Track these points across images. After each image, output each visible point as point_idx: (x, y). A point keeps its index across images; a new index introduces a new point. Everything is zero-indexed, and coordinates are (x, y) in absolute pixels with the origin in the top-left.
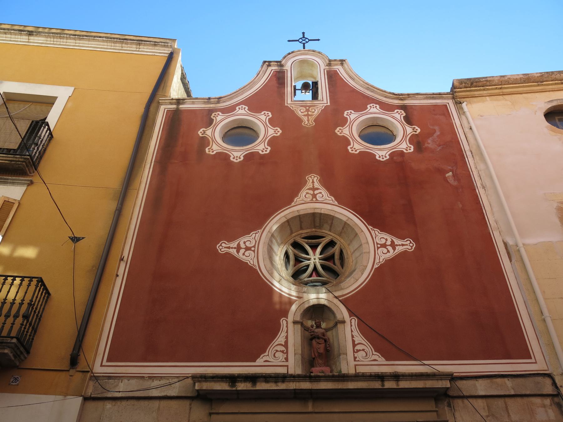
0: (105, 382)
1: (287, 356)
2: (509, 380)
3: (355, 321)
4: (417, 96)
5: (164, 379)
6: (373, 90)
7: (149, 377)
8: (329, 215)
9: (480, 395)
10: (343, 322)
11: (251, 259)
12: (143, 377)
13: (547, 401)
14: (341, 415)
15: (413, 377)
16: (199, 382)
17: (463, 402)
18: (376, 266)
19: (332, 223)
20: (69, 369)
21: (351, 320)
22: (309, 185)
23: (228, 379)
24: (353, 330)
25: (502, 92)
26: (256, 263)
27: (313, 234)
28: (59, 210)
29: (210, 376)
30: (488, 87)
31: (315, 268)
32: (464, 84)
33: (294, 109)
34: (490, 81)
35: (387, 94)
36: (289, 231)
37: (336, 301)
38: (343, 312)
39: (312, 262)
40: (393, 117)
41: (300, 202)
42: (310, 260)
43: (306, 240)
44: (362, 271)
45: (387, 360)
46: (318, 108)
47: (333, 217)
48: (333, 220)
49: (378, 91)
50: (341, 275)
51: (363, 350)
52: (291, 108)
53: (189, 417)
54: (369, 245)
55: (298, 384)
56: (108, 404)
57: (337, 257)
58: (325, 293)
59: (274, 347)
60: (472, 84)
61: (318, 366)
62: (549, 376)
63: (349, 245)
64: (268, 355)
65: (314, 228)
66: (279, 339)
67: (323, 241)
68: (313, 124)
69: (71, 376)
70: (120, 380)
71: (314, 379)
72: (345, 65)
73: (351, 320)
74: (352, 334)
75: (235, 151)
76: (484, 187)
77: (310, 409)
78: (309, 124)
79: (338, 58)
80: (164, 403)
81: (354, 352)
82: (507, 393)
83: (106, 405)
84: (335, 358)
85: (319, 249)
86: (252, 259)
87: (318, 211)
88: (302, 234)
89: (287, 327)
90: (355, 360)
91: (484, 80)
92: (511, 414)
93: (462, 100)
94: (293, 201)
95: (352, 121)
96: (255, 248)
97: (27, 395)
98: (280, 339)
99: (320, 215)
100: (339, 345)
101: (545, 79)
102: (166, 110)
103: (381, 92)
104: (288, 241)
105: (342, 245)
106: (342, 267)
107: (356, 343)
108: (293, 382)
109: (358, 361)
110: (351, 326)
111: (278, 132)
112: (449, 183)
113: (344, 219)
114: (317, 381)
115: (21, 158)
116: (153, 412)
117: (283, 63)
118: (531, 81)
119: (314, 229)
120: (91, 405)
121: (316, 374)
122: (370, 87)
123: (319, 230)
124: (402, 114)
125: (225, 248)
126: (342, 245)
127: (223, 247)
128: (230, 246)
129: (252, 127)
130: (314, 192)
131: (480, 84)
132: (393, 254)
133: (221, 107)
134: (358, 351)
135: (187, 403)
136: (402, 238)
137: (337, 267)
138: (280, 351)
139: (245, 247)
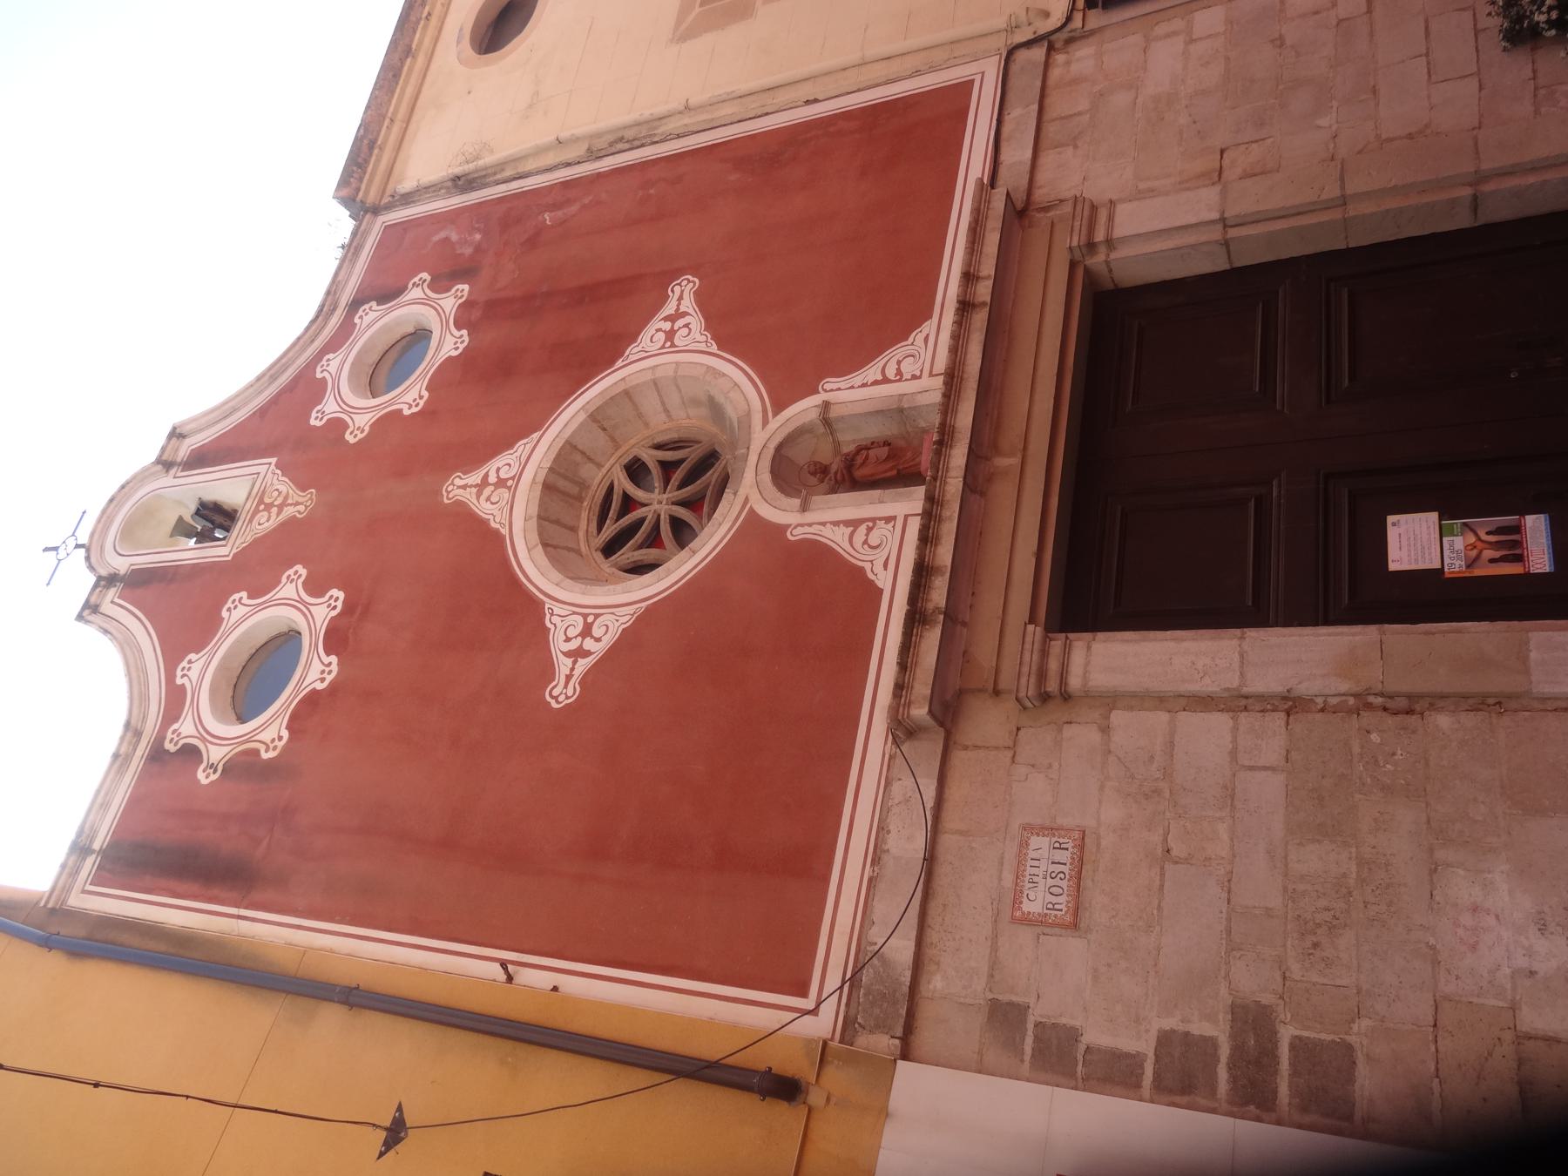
0: (865, 995)
1: (880, 519)
2: (1009, 114)
3: (830, 383)
5: (886, 820)
7: (873, 863)
8: (559, 451)
9: (1031, 157)
10: (826, 405)
11: (617, 621)
12: (870, 880)
15: (976, 248)
18: (714, 348)
19: (583, 453)
20: (807, 1109)
21: (825, 391)
22: (469, 496)
24: (850, 385)
26: (631, 609)
27: (597, 509)
28: (276, 1112)
31: (682, 503)
33: (249, 539)
35: (306, 337)
36: (572, 555)
38: (804, 409)
39: (667, 507)
40: (369, 326)
41: (504, 515)
42: (659, 516)
44: (717, 375)
45: (929, 317)
46: (272, 484)
47: (568, 442)
50: (713, 444)
51: (899, 363)
52: (244, 545)
53: (997, 748)
54: (657, 366)
55: (952, 473)
56: (931, 987)
59: (855, 550)
60: (359, 166)
61: (917, 460)
62: (1011, 52)
63: (646, 425)
64: (871, 561)
65: (582, 503)
66: (838, 539)
67: (619, 484)
68: (312, 493)
71: (946, 437)
72: (185, 430)
73: (825, 391)
74: (859, 387)
75: (303, 678)
78: (307, 501)
80: (951, 819)
81: (900, 380)
82: (1034, 115)
84: (907, 432)
85: (638, 494)
86: (618, 618)
87: (541, 478)
88: (587, 531)
89: (810, 525)
90: (920, 377)
92: (1076, 111)
93: (389, 191)
94: (497, 532)
95: (341, 408)
98: (837, 538)
99: (553, 473)
100: (877, 412)
102: (117, 600)
103: (297, 348)
104: (596, 562)
105: (642, 443)
106: (698, 442)
108: (945, 483)
109: (921, 371)
110: (839, 389)
113: (582, 416)
114: (953, 433)
116: (972, 848)
117: (104, 573)
119: (585, 504)
120: (925, 1037)
121: (936, 430)
122: (272, 372)
123: (591, 493)
124: (241, 598)
125: (566, 687)
126: (642, 443)
127: (562, 691)
128: (567, 676)
130: (491, 484)
132: (695, 316)
134: (899, 372)
135: (959, 758)
136: (664, 299)
137: (692, 455)
138: (867, 535)
139: (580, 639)
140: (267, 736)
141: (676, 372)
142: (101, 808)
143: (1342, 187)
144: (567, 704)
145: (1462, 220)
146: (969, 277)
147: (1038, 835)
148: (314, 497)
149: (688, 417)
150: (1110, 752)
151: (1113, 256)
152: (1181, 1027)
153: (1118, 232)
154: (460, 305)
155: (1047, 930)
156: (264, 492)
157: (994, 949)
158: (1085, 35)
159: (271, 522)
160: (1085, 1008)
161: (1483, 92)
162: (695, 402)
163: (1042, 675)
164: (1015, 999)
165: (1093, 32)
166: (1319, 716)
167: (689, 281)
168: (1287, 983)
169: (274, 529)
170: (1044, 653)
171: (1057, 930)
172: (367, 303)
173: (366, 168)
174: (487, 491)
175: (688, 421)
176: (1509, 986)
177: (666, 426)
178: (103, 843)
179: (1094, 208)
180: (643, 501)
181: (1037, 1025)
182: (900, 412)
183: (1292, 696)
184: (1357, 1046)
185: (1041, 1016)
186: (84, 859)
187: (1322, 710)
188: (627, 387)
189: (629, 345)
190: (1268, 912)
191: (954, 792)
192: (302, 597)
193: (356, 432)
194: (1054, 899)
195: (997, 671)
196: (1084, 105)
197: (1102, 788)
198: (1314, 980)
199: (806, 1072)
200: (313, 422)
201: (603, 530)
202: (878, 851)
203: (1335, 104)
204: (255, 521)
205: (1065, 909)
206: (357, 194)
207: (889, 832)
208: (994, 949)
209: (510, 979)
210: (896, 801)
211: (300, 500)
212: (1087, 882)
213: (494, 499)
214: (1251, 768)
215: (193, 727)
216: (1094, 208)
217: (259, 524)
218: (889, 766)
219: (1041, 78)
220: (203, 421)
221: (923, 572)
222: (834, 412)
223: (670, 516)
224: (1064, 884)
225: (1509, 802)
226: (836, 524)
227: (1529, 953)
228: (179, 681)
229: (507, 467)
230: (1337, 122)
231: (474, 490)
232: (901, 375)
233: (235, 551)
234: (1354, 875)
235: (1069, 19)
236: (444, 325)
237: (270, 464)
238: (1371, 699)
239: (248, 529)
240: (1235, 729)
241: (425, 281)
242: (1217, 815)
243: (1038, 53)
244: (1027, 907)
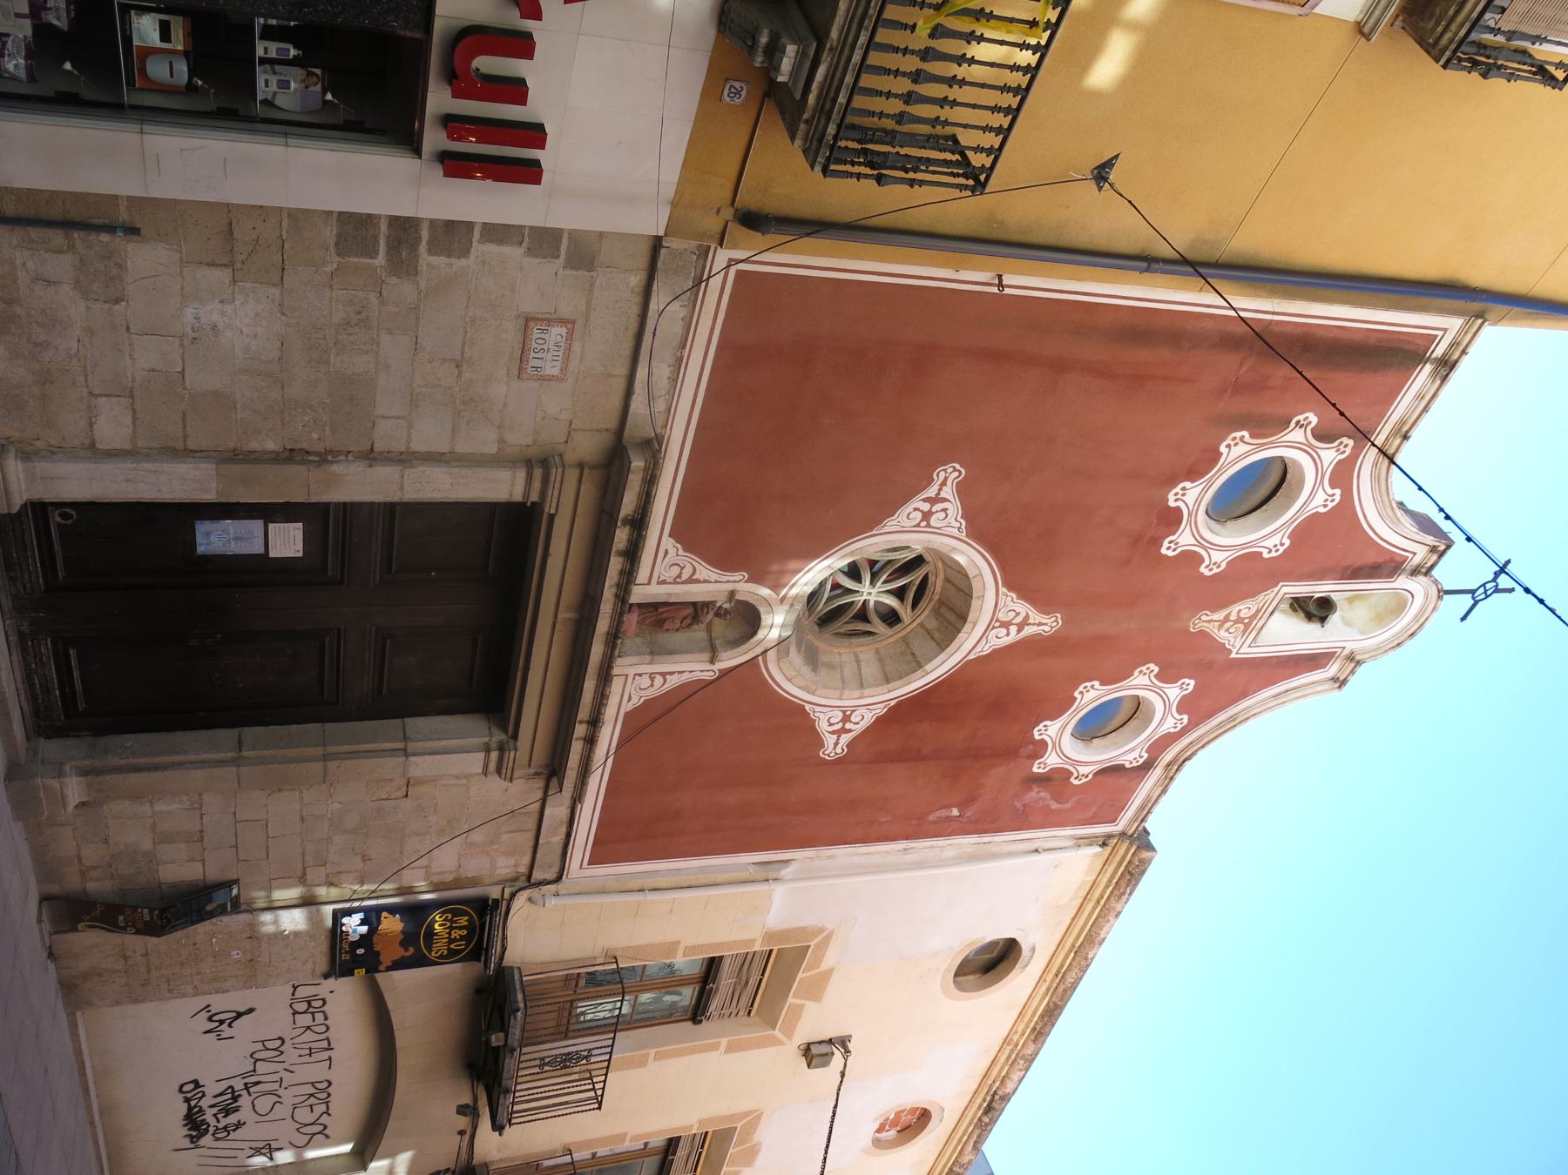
0: (690, 273)
1: (670, 583)
3: (708, 676)
4: (1161, 788)
6: (1221, 728)
7: (682, 358)
10: (712, 662)
13: (523, 869)
14: (545, 655)
16: (646, 469)
17: (539, 788)
18: (807, 707)
19: (933, 639)
20: (735, 205)
21: (713, 671)
22: (1035, 616)
23: (639, 516)
25: (1090, 900)
29: (652, 491)
30: (1111, 888)
31: (849, 591)
32: (1137, 863)
33: (1261, 597)
34: (1120, 898)
35: (1195, 748)
37: (758, 650)
38: (731, 659)
43: (918, 582)
46: (1236, 638)
47: (943, 650)
48: (938, 645)
49: (1213, 736)
50: (819, 632)
56: (638, 278)
57: (862, 627)
58: (780, 636)
62: (559, 879)
63: (877, 652)
64: (678, 555)
69: (718, 211)
70: (686, 303)
73: (713, 671)
76: (905, 849)
77: (562, 615)
79: (1353, 680)
80: (619, 385)
83: (636, 275)
84: (650, 634)
85: (891, 601)
87: (967, 627)
88: (936, 577)
89: (728, 581)
90: (635, 675)
91: (1128, 891)
96: (925, 527)
97: (692, 123)
98: (705, 571)
101: (1077, 959)
102: (1410, 556)
107: (667, 676)
108: (613, 610)
110: (702, 671)
111: (1169, 548)
112: (940, 809)
113: (928, 667)
115: (1451, 41)
118: (1085, 943)
119: (937, 597)
122: (1234, 723)
128: (945, 485)
129: (1264, 507)
131: (1123, 884)
133: (1364, 457)
134: (652, 679)
135: (613, 424)
136: (850, 745)
137: (840, 625)
138: (681, 573)
140: (1242, 448)
141: (842, 693)
142: (1423, 396)
143: (325, 766)
144: (945, 465)
145: (251, 733)
146: (591, 741)
147: (553, 376)
148: (1192, 626)
149: (840, 654)
150: (498, 427)
151: (487, 739)
152: (452, 260)
153: (481, 755)
154: (1042, 757)
155: (548, 316)
156: (1244, 632)
157: (589, 303)
158: (502, 882)
159: (1237, 609)
160: (522, 269)
161: (233, 810)
162: (830, 666)
163: (545, 480)
164: (574, 272)
165: (498, 883)
166: (352, 449)
167: (828, 755)
168: (379, 289)
169: (1234, 603)
170: (543, 494)
171: (540, 316)
172: (1134, 767)
173: (1125, 870)
174: (1019, 620)
175: (841, 651)
176: (236, 294)
177: (861, 649)
178: (1422, 367)
179: (499, 771)
180: (885, 596)
181: (558, 256)
182: (656, 651)
183: (369, 461)
184: (334, 255)
185: (554, 263)
186: (1444, 355)
187: (349, 452)
188: (886, 686)
189: (883, 715)
190: (390, 332)
191: (616, 401)
192: (1206, 553)
193: (1148, 672)
194: (542, 336)
195: (580, 481)
196: (505, 837)
197: (505, 405)
198: (360, 292)
199: (735, 229)
200: (1192, 682)
201: (920, 579)
202: (677, 365)
203: (329, 816)
204: (1254, 611)
205: (535, 329)
206: (1135, 852)
207: (669, 378)
208: (589, 303)
209: (1000, 277)
210: (662, 398)
211: (1206, 624)
212: (518, 347)
213: (1013, 614)
214: (398, 418)
215: (1322, 457)
216: (499, 771)
217: (1250, 608)
218: (667, 422)
219: (537, 860)
220: (1309, 691)
221: (632, 554)
222: (707, 656)
223: (861, 583)
224: (534, 345)
225: (232, 398)
226: (706, 581)
227: (223, 313)
228: (1338, 492)
229: (999, 636)
230: (328, 805)
231: (1031, 621)
232: (650, 677)
233: (1276, 589)
234: (332, 355)
235: (513, 895)
236: (1057, 745)
237: (1237, 653)
238: (317, 459)
239: (1261, 606)
240: (408, 441)
241: (1076, 778)
242: (422, 389)
243: (538, 875)
244: (563, 331)
